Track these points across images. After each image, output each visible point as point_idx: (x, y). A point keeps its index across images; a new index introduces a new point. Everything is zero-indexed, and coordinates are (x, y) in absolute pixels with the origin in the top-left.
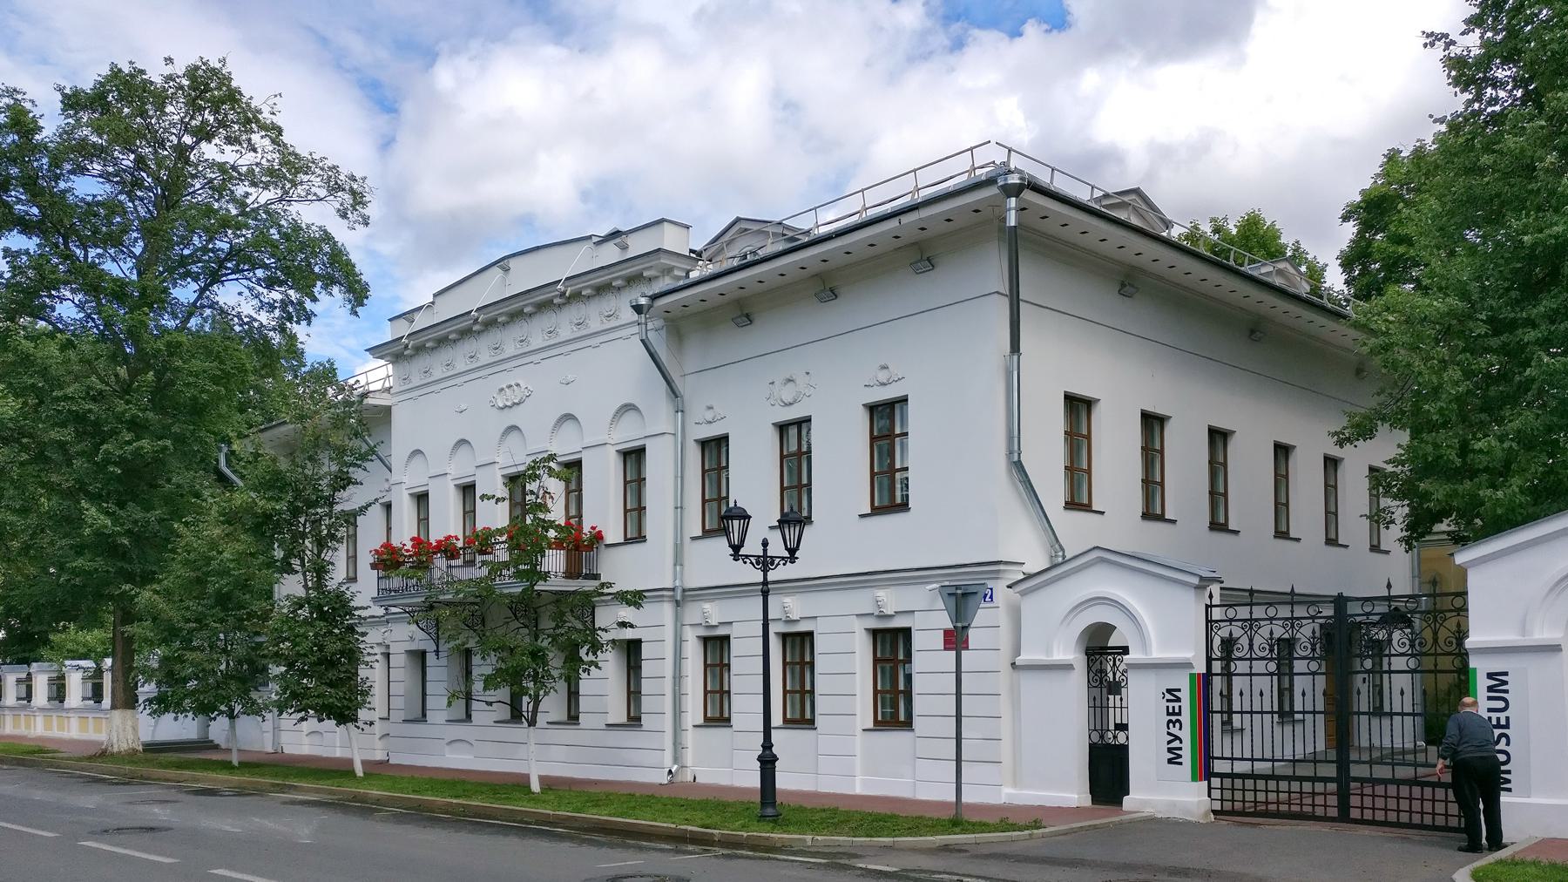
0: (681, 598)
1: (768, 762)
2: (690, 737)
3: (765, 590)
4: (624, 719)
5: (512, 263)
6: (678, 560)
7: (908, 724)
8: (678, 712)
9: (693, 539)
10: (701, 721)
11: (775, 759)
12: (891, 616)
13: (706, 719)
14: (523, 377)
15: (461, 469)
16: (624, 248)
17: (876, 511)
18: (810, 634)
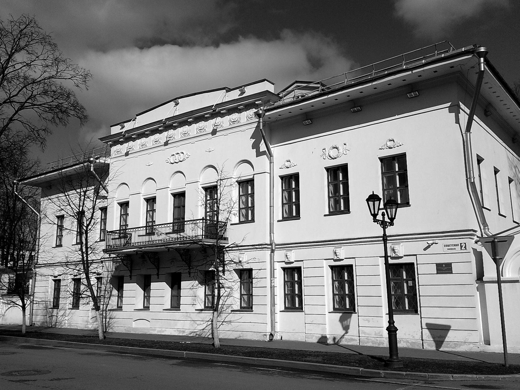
0: (272, 247)
1: (392, 330)
2: (279, 316)
3: (385, 238)
4: (142, 308)
5: (180, 100)
6: (271, 231)
7: (300, 309)
8: (273, 304)
9: (279, 221)
10: (283, 309)
11: (396, 329)
12: (293, 263)
13: (285, 308)
14: (186, 148)
15: (148, 190)
16: (243, 93)
17: (331, 214)
18: (351, 266)
